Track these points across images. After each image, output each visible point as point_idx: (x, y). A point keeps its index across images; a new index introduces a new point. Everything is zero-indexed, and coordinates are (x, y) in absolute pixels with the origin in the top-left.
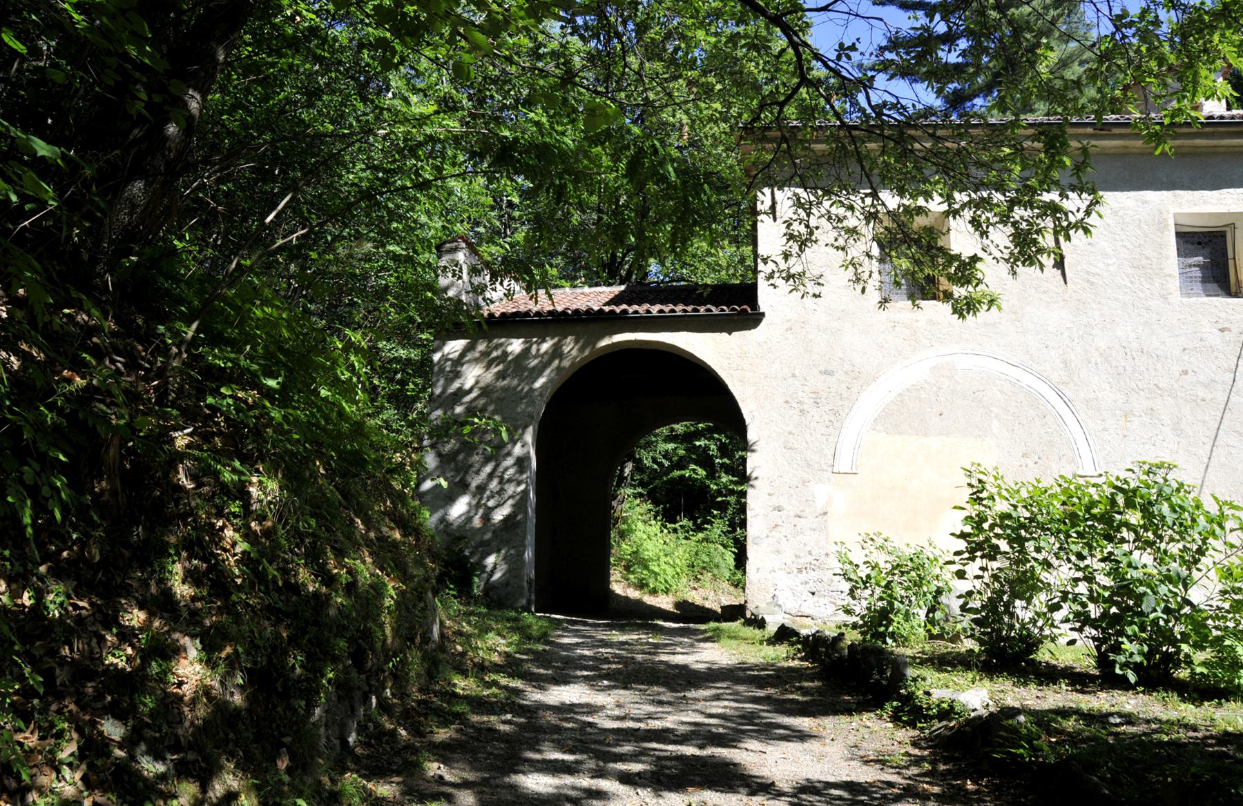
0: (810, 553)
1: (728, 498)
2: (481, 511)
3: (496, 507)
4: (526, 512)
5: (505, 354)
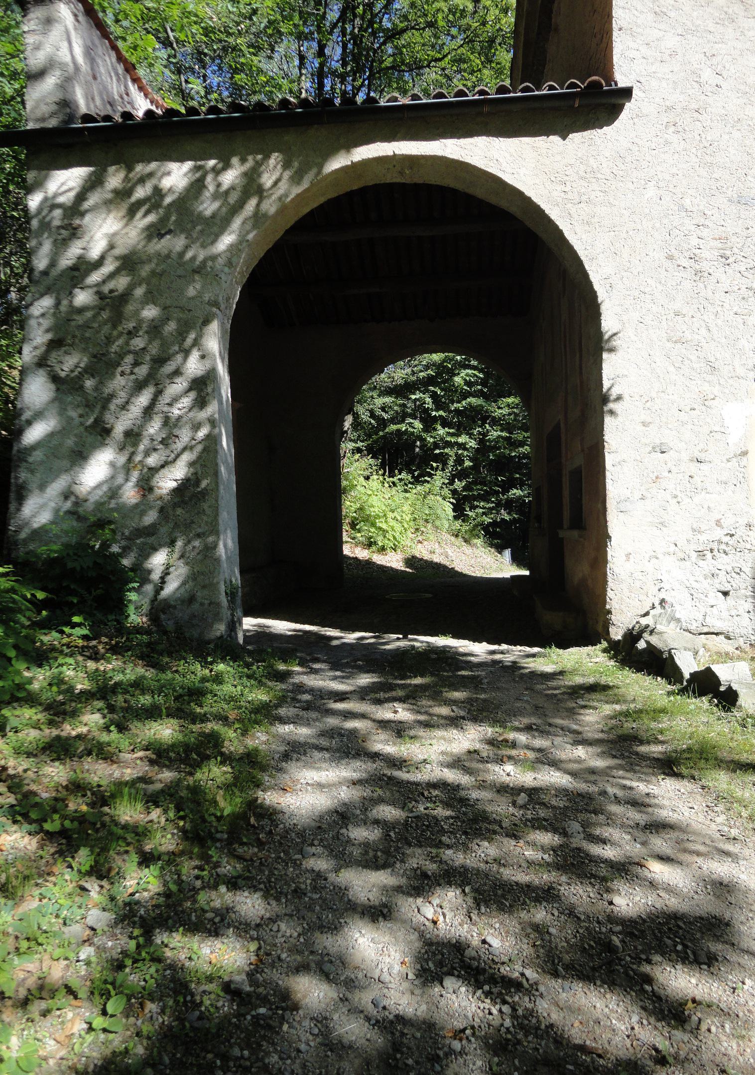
0: (718, 523)
1: (446, 451)
2: (135, 475)
3: (163, 466)
4: (216, 474)
5: (158, 192)
